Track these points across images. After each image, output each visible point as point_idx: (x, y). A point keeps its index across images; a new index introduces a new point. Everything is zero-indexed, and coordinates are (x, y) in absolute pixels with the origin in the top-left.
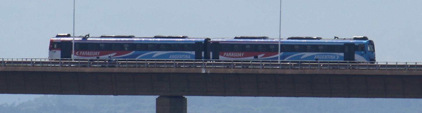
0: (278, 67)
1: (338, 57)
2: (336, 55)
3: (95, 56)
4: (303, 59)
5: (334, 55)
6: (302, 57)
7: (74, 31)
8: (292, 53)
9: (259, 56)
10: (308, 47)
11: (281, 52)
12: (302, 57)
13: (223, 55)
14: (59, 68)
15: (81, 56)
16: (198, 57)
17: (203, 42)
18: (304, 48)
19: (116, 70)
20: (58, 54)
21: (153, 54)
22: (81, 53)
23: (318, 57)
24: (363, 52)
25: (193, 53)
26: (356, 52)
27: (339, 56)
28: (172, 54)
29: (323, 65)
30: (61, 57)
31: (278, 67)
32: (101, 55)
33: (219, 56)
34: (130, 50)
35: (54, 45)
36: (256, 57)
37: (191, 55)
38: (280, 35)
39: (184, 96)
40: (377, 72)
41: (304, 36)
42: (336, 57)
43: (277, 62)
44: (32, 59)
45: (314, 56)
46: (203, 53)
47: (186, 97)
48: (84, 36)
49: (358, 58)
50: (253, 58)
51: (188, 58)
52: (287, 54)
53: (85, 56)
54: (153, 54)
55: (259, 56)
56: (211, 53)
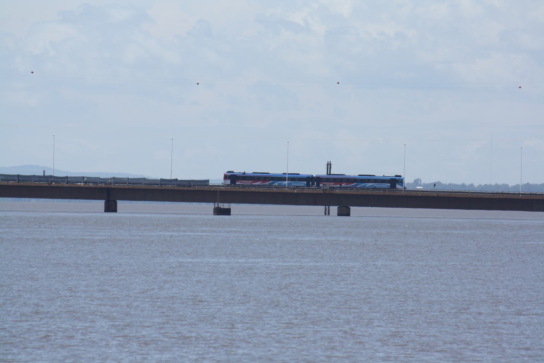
0: (286, 189)
1: (387, 186)
2: (386, 185)
3: (250, 183)
4: (367, 187)
5: (385, 185)
6: (367, 186)
7: (521, 177)
8: (277, 181)
9: (343, 185)
10: (371, 180)
11: (288, 181)
12: (367, 186)
13: (238, 182)
14: (229, 189)
15: (242, 183)
16: (308, 185)
17: (311, 177)
18: (369, 181)
19: (192, 189)
20: (228, 182)
21: (366, 185)
22: (242, 181)
23: (376, 186)
24: (401, 184)
25: (305, 182)
26: (397, 183)
27: (388, 185)
28: (293, 183)
29: (242, 187)
30: (307, 185)
31: (286, 189)
32: (253, 182)
33: (396, 186)
34: (269, 180)
35: (226, 177)
36: (341, 185)
37: (304, 184)
38: (521, 178)
39: (349, 207)
40: (78, 186)
41: (260, 172)
42: (386, 186)
43: (286, 186)
44: (469, 191)
45: (373, 185)
46: (311, 183)
47: (350, 207)
48: (243, 172)
49: (398, 186)
50: (339, 186)
51: (303, 185)
52: (358, 184)
53: (244, 183)
54: (366, 185)
55: (343, 185)
56: (315, 183)
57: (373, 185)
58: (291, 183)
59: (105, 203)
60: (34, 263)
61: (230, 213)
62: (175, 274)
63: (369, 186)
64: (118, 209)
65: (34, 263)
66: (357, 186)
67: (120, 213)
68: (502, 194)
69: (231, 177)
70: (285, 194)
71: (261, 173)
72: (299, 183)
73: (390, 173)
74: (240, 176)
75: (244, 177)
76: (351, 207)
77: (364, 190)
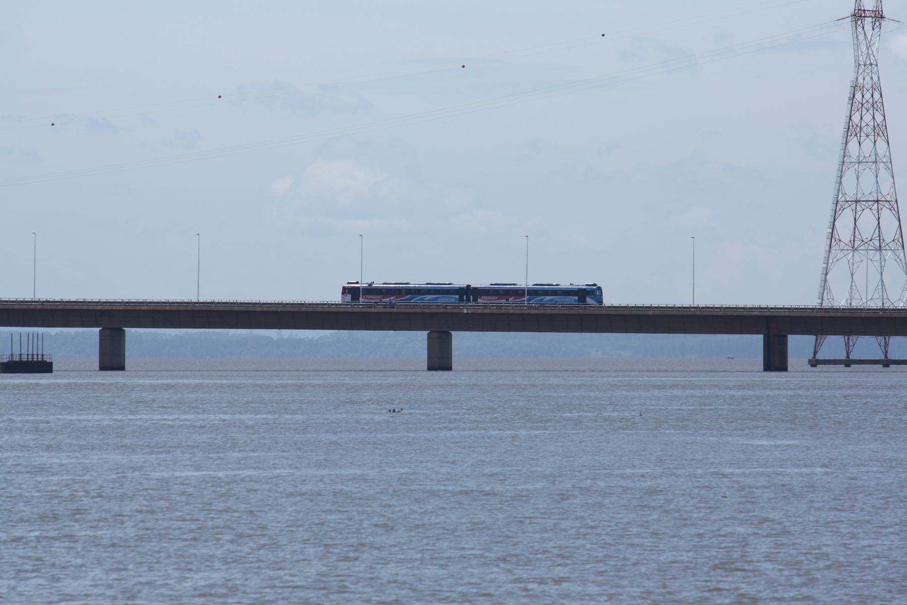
16: (461, 299)
18: (546, 293)
19: (395, 310)
20: (349, 297)
25: (457, 297)
28: (440, 297)
32: (383, 298)
33: (586, 300)
35: (345, 291)
36: (507, 300)
37: (456, 299)
46: (465, 297)
47: (124, 329)
49: (589, 300)
51: (453, 300)
52: (413, 296)
57: (553, 299)
58: (437, 298)
59: (429, 337)
60: (664, 591)
61: (449, 357)
62: (14, 570)
63: (547, 301)
64: (789, 367)
65: (664, 591)
66: (411, 300)
67: (791, 372)
68: (84, 302)
69: (351, 291)
70: (508, 316)
71: (437, 284)
72: (446, 297)
73: (580, 281)
74: (572, 291)
75: (370, 291)
76: (127, 330)
77: (494, 306)
